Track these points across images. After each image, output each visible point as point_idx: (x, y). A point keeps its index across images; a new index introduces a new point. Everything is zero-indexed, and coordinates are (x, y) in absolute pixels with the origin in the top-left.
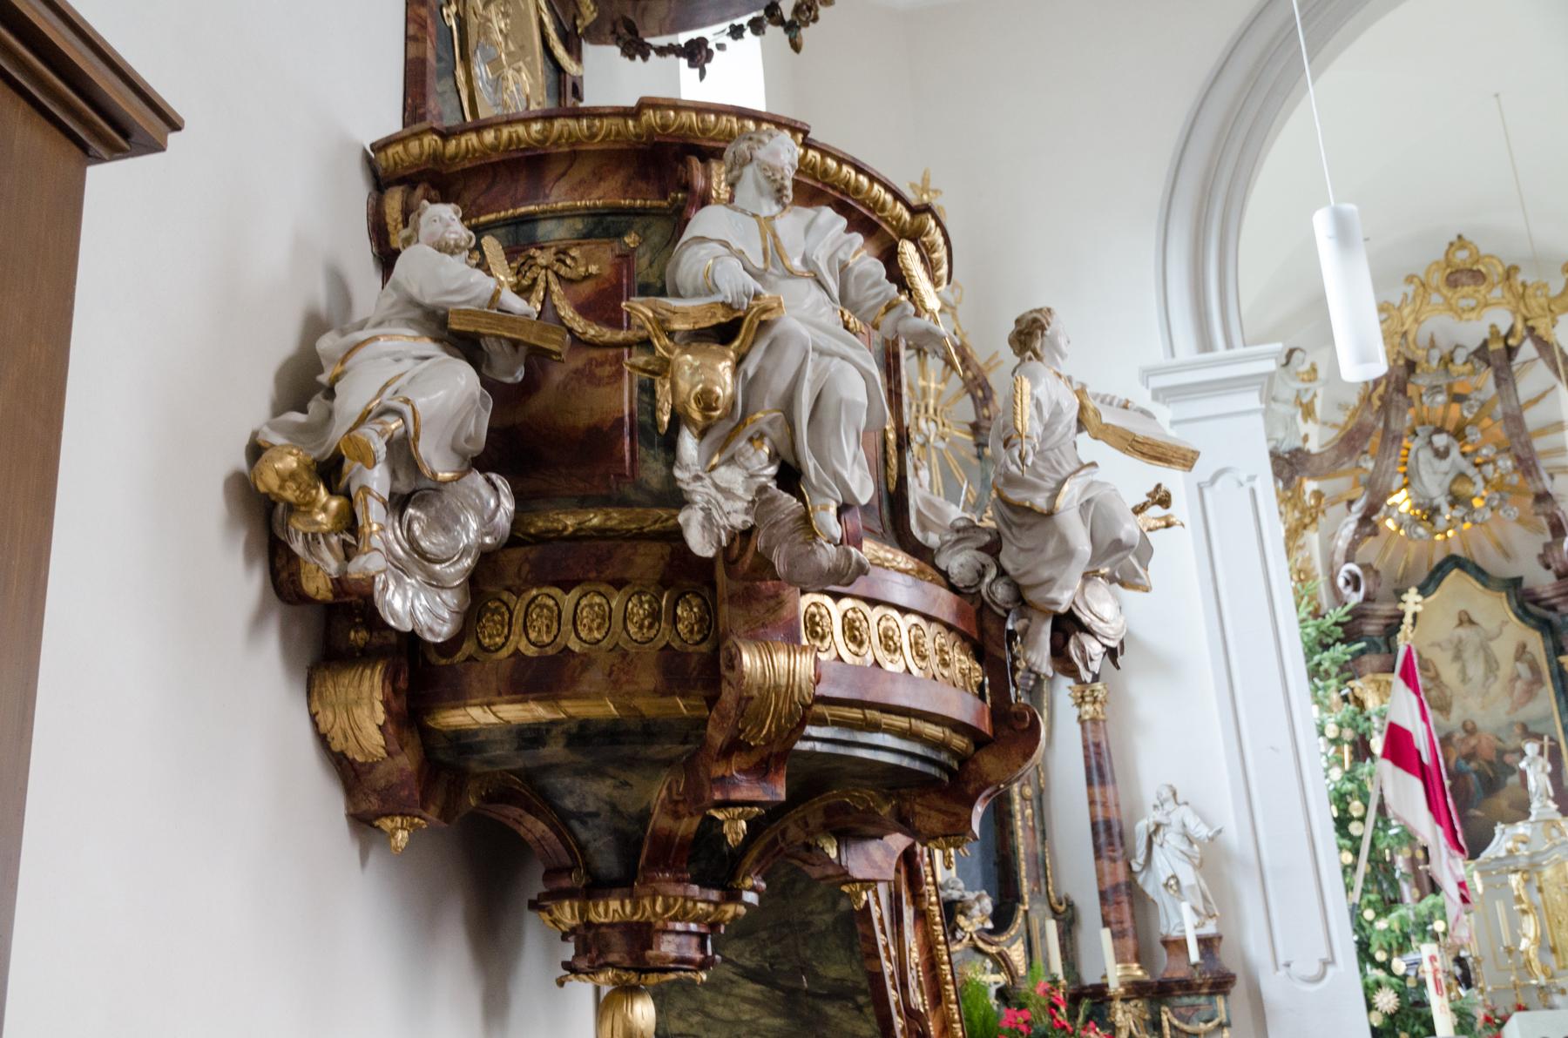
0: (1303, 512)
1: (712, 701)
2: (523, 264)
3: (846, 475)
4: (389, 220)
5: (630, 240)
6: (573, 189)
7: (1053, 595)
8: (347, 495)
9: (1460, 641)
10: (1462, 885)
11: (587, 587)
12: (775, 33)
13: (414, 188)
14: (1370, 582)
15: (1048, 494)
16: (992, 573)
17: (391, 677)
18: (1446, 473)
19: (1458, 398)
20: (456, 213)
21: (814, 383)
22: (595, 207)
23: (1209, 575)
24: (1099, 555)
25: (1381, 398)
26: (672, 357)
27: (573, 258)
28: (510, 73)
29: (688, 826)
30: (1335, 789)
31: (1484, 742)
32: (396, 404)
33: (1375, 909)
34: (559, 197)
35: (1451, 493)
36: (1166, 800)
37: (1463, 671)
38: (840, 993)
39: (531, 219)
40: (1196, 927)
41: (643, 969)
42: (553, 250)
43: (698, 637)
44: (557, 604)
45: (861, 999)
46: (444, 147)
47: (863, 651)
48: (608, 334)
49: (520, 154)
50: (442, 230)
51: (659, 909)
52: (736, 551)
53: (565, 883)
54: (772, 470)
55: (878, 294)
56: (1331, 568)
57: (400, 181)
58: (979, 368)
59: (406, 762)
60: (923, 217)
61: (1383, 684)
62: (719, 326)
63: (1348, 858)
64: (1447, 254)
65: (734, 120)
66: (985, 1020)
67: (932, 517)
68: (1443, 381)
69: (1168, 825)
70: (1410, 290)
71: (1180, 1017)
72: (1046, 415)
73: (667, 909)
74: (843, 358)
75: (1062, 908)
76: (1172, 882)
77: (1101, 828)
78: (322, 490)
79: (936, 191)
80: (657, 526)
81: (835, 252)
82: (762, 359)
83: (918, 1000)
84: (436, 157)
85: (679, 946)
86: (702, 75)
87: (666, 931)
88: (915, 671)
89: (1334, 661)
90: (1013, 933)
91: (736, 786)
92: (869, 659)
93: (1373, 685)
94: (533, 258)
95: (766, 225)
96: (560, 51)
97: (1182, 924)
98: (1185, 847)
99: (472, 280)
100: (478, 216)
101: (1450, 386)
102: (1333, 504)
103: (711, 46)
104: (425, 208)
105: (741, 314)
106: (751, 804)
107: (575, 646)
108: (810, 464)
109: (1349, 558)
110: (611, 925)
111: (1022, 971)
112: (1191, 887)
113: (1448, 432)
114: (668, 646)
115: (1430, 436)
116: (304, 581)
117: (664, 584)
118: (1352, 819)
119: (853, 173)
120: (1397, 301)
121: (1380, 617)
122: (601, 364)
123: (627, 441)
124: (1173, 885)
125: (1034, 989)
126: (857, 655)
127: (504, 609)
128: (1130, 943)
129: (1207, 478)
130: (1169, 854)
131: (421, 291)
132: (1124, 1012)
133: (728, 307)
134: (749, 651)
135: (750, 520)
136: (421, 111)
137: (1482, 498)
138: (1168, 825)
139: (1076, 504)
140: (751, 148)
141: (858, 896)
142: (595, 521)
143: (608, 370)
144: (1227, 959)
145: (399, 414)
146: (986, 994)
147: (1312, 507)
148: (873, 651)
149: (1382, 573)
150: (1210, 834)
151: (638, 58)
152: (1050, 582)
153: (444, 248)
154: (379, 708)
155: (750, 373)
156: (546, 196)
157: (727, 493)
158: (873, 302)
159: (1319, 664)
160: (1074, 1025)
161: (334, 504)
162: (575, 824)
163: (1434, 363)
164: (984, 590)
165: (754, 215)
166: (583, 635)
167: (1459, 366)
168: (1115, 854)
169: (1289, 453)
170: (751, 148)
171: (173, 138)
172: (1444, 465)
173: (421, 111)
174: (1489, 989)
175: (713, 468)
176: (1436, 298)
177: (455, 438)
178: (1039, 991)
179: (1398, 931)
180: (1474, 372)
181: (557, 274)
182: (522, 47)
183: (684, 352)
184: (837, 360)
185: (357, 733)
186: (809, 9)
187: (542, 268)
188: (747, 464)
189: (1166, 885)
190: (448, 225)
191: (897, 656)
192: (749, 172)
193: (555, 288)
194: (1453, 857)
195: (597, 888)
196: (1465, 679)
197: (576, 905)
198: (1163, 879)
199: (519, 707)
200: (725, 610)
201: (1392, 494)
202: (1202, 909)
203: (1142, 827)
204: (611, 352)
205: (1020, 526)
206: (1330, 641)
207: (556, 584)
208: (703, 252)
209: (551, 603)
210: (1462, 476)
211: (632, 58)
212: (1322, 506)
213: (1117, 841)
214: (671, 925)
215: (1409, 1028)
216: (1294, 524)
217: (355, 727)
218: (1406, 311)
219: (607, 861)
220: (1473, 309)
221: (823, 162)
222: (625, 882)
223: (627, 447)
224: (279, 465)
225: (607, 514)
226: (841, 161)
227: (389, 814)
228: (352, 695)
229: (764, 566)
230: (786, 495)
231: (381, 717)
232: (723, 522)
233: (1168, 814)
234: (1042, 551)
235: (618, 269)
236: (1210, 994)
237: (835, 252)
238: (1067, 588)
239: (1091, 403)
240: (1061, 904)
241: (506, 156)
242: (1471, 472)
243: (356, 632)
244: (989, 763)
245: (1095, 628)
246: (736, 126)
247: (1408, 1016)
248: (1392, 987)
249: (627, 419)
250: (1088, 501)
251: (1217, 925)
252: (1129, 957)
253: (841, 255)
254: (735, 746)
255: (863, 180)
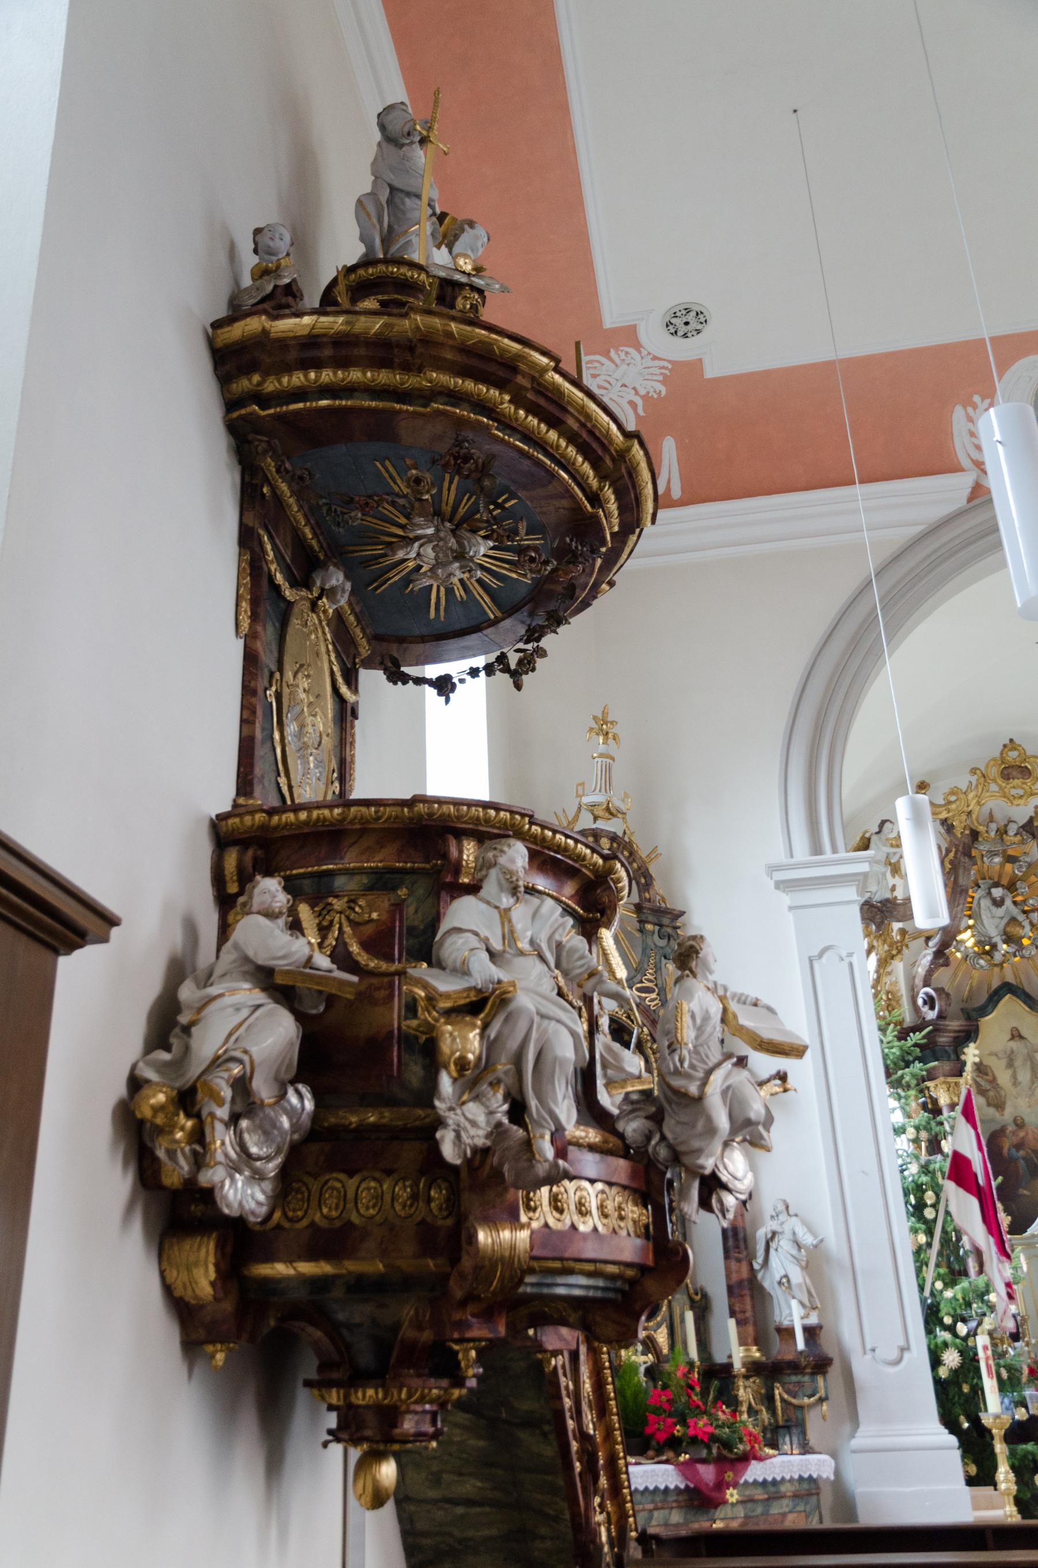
0: (891, 946)
1: (455, 1260)
2: (323, 909)
3: (557, 1111)
4: (227, 872)
5: (402, 892)
6: (362, 853)
7: (701, 1161)
8: (198, 1116)
9: (1012, 1052)
10: (1008, 1285)
11: (365, 1173)
12: (503, 679)
13: (247, 848)
14: (943, 1003)
15: (698, 1083)
16: (656, 1138)
17: (220, 1247)
18: (1002, 918)
19: (1012, 859)
20: (280, 883)
21: (538, 1040)
22: (377, 867)
23: (816, 1031)
24: (734, 1130)
25: (951, 862)
26: (438, 1025)
27: (360, 906)
28: (309, 720)
29: (427, 1336)
30: (913, 1181)
31: (1030, 1136)
32: (238, 1054)
33: (943, 1281)
34: (350, 860)
35: (1005, 933)
36: (781, 1212)
37: (1014, 1076)
38: (530, 1423)
39: (330, 874)
40: (802, 1318)
41: (390, 1440)
42: (346, 899)
43: (445, 1213)
44: (343, 1186)
45: (547, 1428)
46: (270, 821)
47: (563, 1217)
48: (384, 966)
49: (325, 828)
50: (270, 900)
51: (403, 1396)
52: (477, 1163)
53: (335, 1375)
54: (506, 1107)
55: (582, 966)
56: (913, 990)
57: (235, 842)
58: (644, 862)
59: (228, 1306)
60: (612, 862)
61: (952, 1085)
62: (471, 1003)
63: (922, 1239)
64: (1002, 753)
65: (481, 810)
66: (636, 1395)
67: (611, 1060)
68: (999, 848)
69: (782, 1233)
70: (974, 779)
71: (788, 1392)
72: (698, 1021)
73: (410, 1395)
74: (558, 1021)
75: (698, 1298)
76: (784, 1280)
77: (730, 1234)
78: (182, 1115)
79: (612, 723)
80: (417, 1123)
81: (553, 933)
82: (502, 1026)
83: (589, 1418)
84: (264, 827)
85: (417, 1423)
86: (447, 701)
87: (408, 1411)
88: (600, 1228)
89: (913, 1075)
90: (659, 1319)
91: (469, 1327)
92: (568, 1223)
93: (944, 1086)
94: (331, 904)
95: (505, 915)
96: (344, 690)
97: (791, 1315)
98: (794, 1252)
99: (293, 949)
100: (292, 870)
101: (1004, 851)
102: (915, 938)
103: (455, 680)
104: (258, 883)
105: (487, 994)
106: (480, 1340)
107: (355, 1218)
108: (533, 1103)
109: (926, 984)
110: (367, 1407)
111: (665, 1351)
112: (799, 1285)
113: (1003, 886)
114: (423, 1222)
115: (989, 889)
116: (163, 1177)
117: (422, 1172)
118: (925, 1205)
119: (563, 838)
120: (964, 787)
121: (950, 1031)
122: (378, 989)
123: (396, 1048)
124: (785, 1282)
125: (675, 1370)
126: (559, 1220)
127: (304, 1189)
128: (750, 1329)
129: (816, 953)
130: (782, 1257)
131: (256, 954)
132: (745, 1387)
133: (479, 991)
134: (484, 1230)
135: (488, 1143)
136: (250, 777)
137: (1029, 938)
138: (782, 1233)
139: (718, 1090)
140: (495, 856)
141: (549, 1362)
142: (372, 1119)
143: (382, 994)
144: (828, 1348)
145: (240, 1061)
146: (637, 1374)
147: (898, 942)
148: (570, 1216)
149: (952, 997)
150: (815, 1242)
151: (399, 683)
152: (699, 1152)
153: (270, 915)
154: (212, 1269)
155: (492, 1036)
156: (342, 858)
157: (474, 1124)
158: (578, 971)
159: (902, 1077)
160: (705, 1403)
161: (189, 1124)
162: (345, 1332)
163: (993, 834)
164: (650, 1149)
165: (496, 907)
166: (362, 1211)
167: (1011, 836)
168: (741, 1256)
169: (880, 902)
170: (495, 856)
171: (115, 932)
172: (1000, 912)
173: (250, 777)
174: (1033, 1341)
175: (464, 1103)
176: (994, 787)
177: (278, 1072)
178: (679, 1374)
179: (961, 1301)
180: (1023, 842)
181: (348, 918)
182: (318, 696)
183: (447, 1023)
184: (553, 1023)
185: (194, 1286)
186: (529, 663)
187: (338, 912)
188: (488, 1103)
189: (780, 1283)
190: (275, 897)
191: (588, 1218)
192: (493, 873)
193: (347, 929)
194: (1002, 1262)
195: (358, 1378)
196: (1015, 1083)
197: (342, 1392)
198: (778, 1278)
199: (313, 1264)
200: (466, 1196)
201: (960, 932)
202: (807, 1303)
203: (762, 1234)
204: (386, 980)
205: (678, 1104)
206: (911, 1058)
207: (343, 1171)
208: (460, 941)
209: (338, 1185)
210: (1013, 920)
211: (395, 683)
212: (906, 940)
213: (742, 1245)
214: (413, 1407)
215: (970, 1381)
216: (884, 955)
217: (193, 1282)
218: (971, 795)
219: (366, 1358)
220: (1021, 797)
221: (542, 833)
222: (378, 1375)
223: (395, 1053)
224: (153, 1101)
225: (381, 1113)
226: (555, 832)
227: (213, 1342)
228: (192, 1258)
229: (497, 1174)
230: (515, 1128)
231: (212, 1275)
232: (468, 1141)
233: (782, 1224)
234: (694, 1126)
235: (392, 915)
236: (813, 1374)
237: (553, 933)
238: (711, 1156)
239: (734, 1006)
240: (697, 1294)
241: (314, 829)
242: (1021, 917)
243: (196, 1206)
244: (651, 1285)
245: (730, 1186)
246: (481, 814)
247: (969, 1371)
248: (957, 1347)
249: (396, 1032)
250: (728, 1088)
251: (819, 1316)
252: (750, 1340)
253: (557, 937)
254: (470, 1298)
255: (570, 842)
